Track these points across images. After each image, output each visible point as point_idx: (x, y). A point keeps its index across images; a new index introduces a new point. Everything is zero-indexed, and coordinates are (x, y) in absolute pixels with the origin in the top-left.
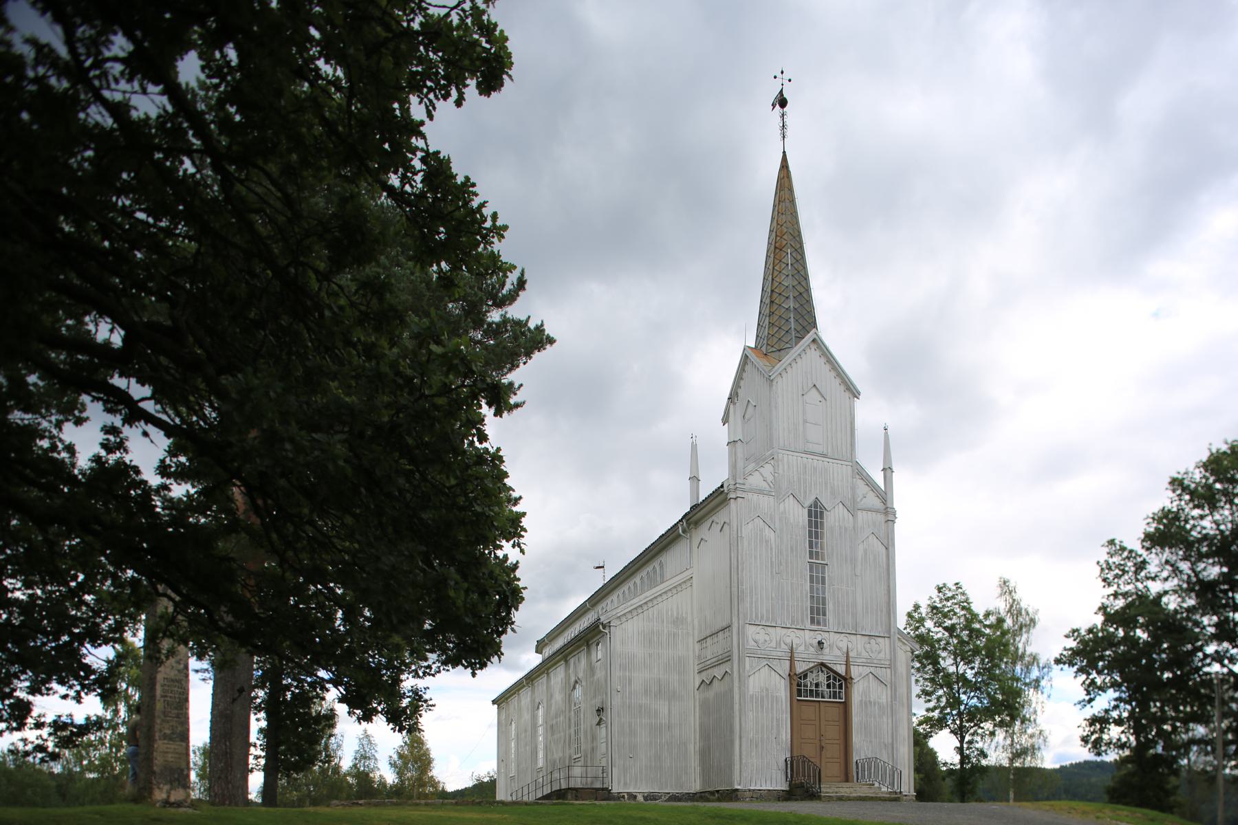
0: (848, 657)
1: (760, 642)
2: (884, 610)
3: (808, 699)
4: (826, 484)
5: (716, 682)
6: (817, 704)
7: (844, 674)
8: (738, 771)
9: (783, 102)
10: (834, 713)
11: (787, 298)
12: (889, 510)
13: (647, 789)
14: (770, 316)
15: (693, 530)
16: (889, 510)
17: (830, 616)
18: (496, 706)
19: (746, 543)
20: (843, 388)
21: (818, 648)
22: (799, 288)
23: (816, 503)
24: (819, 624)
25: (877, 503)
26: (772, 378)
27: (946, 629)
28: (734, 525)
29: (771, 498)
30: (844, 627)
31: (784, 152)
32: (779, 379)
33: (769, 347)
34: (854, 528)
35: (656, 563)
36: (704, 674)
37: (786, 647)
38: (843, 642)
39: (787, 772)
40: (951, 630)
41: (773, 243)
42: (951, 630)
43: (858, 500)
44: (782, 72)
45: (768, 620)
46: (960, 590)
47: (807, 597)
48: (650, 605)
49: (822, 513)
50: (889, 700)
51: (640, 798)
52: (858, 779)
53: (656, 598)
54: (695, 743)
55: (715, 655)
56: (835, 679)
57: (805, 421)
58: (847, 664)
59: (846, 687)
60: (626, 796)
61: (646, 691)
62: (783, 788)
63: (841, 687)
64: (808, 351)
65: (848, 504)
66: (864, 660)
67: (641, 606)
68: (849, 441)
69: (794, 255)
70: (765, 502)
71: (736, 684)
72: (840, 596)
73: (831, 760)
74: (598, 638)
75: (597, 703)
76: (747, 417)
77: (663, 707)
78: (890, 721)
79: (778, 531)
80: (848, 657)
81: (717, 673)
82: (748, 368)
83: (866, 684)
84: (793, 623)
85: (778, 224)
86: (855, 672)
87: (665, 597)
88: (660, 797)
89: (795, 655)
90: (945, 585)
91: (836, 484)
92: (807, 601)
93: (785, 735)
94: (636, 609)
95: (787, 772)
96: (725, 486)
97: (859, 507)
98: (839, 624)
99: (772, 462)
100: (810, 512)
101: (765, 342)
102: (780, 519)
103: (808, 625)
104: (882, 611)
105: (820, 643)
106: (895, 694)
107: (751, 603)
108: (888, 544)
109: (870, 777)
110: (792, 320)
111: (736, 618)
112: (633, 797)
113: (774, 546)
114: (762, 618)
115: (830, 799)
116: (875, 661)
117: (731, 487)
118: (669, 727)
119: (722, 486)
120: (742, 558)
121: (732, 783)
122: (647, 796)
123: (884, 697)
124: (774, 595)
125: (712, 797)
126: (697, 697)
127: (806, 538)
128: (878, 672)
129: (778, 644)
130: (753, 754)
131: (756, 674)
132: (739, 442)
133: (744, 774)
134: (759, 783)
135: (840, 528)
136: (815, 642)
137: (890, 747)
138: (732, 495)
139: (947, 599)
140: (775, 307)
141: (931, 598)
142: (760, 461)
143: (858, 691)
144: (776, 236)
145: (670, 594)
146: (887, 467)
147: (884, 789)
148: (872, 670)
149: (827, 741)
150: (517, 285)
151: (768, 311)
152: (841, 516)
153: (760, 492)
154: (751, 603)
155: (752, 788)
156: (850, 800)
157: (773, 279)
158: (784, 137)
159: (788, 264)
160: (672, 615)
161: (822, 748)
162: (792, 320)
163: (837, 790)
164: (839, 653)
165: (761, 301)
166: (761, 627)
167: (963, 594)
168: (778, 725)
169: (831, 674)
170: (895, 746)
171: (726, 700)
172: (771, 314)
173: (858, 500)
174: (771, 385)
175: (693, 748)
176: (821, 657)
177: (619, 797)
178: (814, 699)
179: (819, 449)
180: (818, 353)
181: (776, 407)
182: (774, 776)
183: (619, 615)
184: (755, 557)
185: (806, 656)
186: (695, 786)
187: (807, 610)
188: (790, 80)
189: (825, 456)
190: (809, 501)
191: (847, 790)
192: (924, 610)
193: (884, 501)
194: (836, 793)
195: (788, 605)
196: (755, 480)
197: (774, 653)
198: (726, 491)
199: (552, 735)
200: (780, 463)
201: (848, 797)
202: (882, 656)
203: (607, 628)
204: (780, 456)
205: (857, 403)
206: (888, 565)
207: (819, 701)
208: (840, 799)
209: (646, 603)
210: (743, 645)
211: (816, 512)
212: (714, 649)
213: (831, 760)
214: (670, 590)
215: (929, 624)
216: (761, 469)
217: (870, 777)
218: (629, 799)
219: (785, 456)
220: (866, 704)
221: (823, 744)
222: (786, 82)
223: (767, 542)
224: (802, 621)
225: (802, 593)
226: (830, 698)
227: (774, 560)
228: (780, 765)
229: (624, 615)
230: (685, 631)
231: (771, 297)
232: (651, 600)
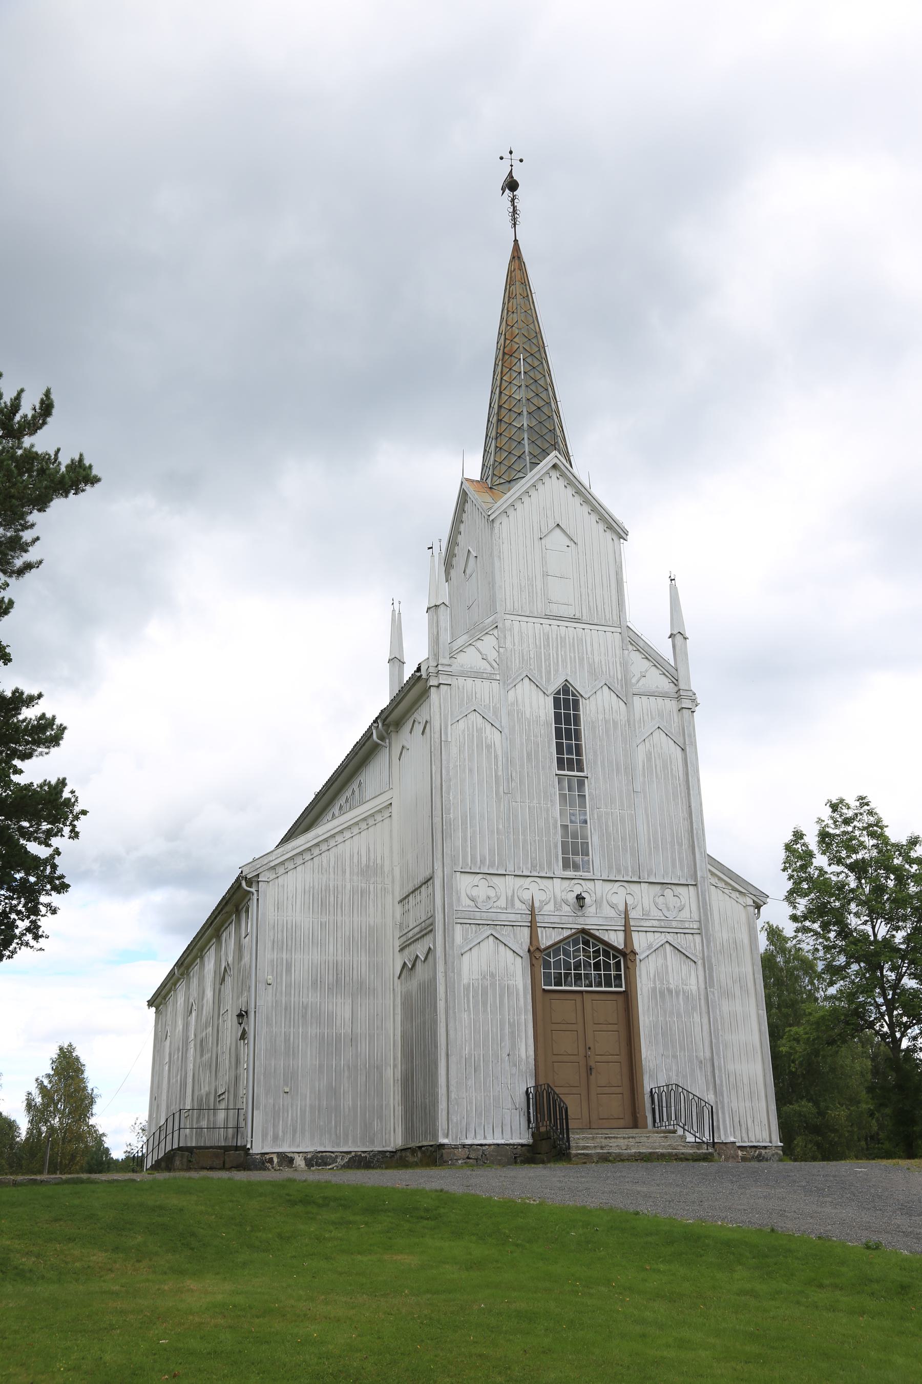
0: (627, 918)
1: (480, 900)
2: (685, 842)
3: (594, 989)
4: (581, 660)
5: (419, 964)
6: (578, 997)
7: (621, 946)
8: (445, 1113)
9: (512, 185)
10: (609, 1010)
11: (519, 414)
12: (682, 693)
13: (310, 1146)
14: (496, 438)
15: (393, 735)
16: (682, 693)
17: (595, 855)
18: (153, 1009)
19: (454, 750)
20: (601, 526)
21: (577, 907)
22: (535, 401)
23: (566, 689)
24: (576, 867)
25: (664, 684)
26: (491, 518)
27: (851, 867)
28: (436, 724)
29: (495, 683)
30: (619, 871)
31: (516, 241)
32: (504, 519)
33: (495, 478)
34: (628, 721)
35: (355, 785)
36: (406, 951)
37: (524, 907)
38: (618, 895)
39: (529, 1113)
40: (859, 868)
41: (502, 348)
42: (859, 868)
43: (634, 681)
44: (511, 152)
45: (492, 865)
46: (866, 807)
47: (556, 827)
48: (324, 847)
49: (576, 703)
50: (702, 986)
51: (300, 1162)
52: (654, 1121)
53: (333, 836)
54: (395, 1066)
55: (418, 922)
56: (606, 954)
57: (546, 575)
58: (627, 931)
59: (626, 967)
60: (275, 1160)
61: (314, 983)
62: (516, 1140)
63: (618, 965)
64: (546, 480)
65: (617, 687)
66: (656, 923)
67: (309, 849)
68: (614, 598)
69: (529, 360)
70: (486, 691)
71: (440, 968)
72: (610, 824)
73: (607, 1090)
74: (245, 902)
75: (241, 1003)
76: (468, 572)
77: (342, 1008)
78: (705, 1020)
79: (506, 731)
80: (627, 918)
81: (420, 949)
82: (468, 507)
83: (660, 961)
84: (533, 867)
85: (507, 325)
86: (640, 942)
87: (347, 834)
88: (334, 1160)
89: (538, 919)
90: (842, 801)
91: (596, 660)
92: (555, 834)
93: (526, 1049)
94: (301, 853)
95: (529, 1113)
96: (423, 669)
97: (635, 691)
98: (610, 868)
99: (495, 632)
100: (557, 702)
101: (490, 473)
102: (509, 714)
103: (559, 871)
104: (680, 845)
105: (580, 898)
106: (711, 977)
107: (464, 839)
108: (685, 743)
109: (669, 1118)
110: (526, 442)
111: (440, 863)
112: (287, 1160)
113: (499, 753)
114: (483, 862)
115: (586, 1159)
116: (674, 924)
117: (431, 670)
118: (353, 1040)
119: (419, 669)
120: (448, 772)
121: (435, 1136)
122: (312, 1159)
123: (693, 980)
124: (501, 827)
125: (411, 1159)
126: (398, 989)
127: (552, 740)
128: (679, 941)
129: (511, 902)
130: (471, 1082)
131: (475, 951)
132: (442, 607)
133: (454, 1118)
134: (480, 1132)
135: (607, 722)
136: (571, 897)
137: (709, 1065)
138: (433, 682)
139: (847, 822)
140: (504, 426)
141: (820, 821)
142: (477, 632)
143: (648, 973)
144: (505, 339)
145: (356, 830)
146: (675, 632)
147: (690, 1138)
148: (670, 938)
149: (598, 1058)
150: (41, 408)
151: (494, 433)
152: (607, 706)
153: (477, 675)
154: (464, 839)
155: (468, 1142)
156: (623, 1160)
157: (501, 393)
158: (515, 224)
159: (520, 373)
160: (359, 861)
161: (590, 1070)
162: (526, 442)
163: (604, 1142)
164: (612, 913)
165: (488, 421)
166: (480, 876)
167: (871, 813)
168: (512, 1034)
169: (601, 946)
170: (716, 1064)
171: (428, 990)
172: (499, 435)
173: (634, 681)
174: (492, 528)
175: (392, 1074)
176: (581, 920)
177: (263, 1162)
178: (574, 988)
179: (569, 612)
180: (562, 483)
181: (499, 557)
182: (507, 1120)
183: (272, 864)
184: (471, 771)
185: (556, 920)
186: (395, 1140)
187: (556, 846)
188: (521, 161)
189: (576, 620)
190: (556, 684)
191: (622, 1143)
192: (812, 841)
193: (675, 682)
194: (602, 1148)
195: (525, 841)
196: (469, 659)
197: (503, 917)
198: (424, 676)
199: (202, 1056)
200: (508, 634)
201: (619, 1155)
202: (685, 914)
203: (254, 885)
204: (508, 623)
205: (625, 545)
206: (687, 774)
207: (581, 992)
208: (605, 1158)
209: (317, 845)
210: (451, 905)
211: (566, 701)
212: (416, 915)
213: (607, 1090)
214: (357, 823)
215: (821, 860)
216: (479, 644)
217: (669, 1118)
218: (280, 1164)
219: (516, 624)
220: (663, 994)
221: (592, 1063)
222: (516, 163)
223: (489, 747)
224: (549, 864)
225: (547, 820)
226: (600, 985)
227: (500, 773)
228: (517, 1100)
229: (282, 863)
230: (379, 886)
231: (498, 413)
232: (326, 840)
